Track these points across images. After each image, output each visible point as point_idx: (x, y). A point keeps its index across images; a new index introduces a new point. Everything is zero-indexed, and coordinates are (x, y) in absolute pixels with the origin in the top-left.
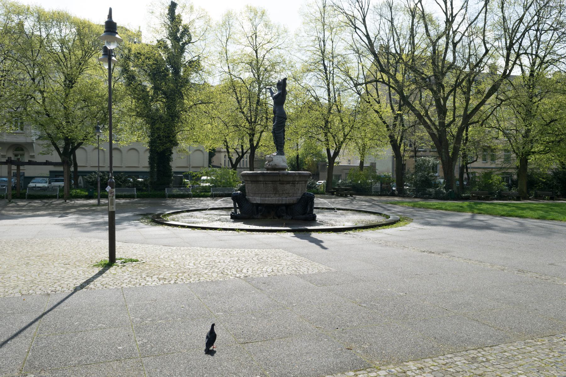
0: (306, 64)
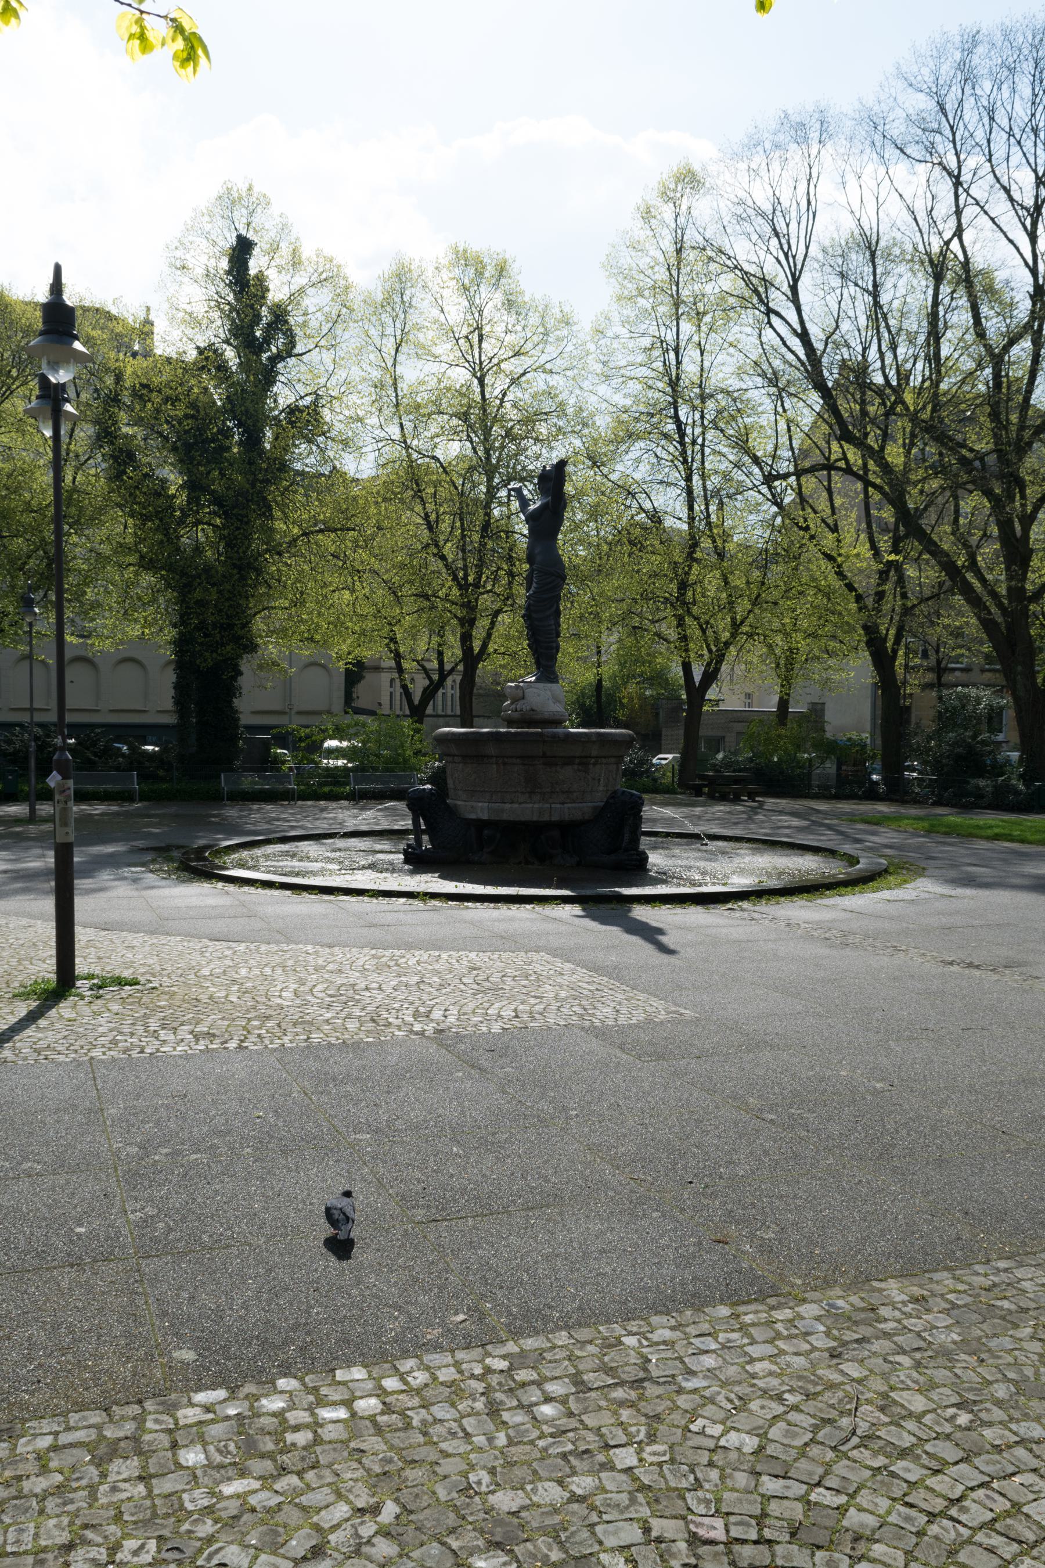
0: (625, 416)
